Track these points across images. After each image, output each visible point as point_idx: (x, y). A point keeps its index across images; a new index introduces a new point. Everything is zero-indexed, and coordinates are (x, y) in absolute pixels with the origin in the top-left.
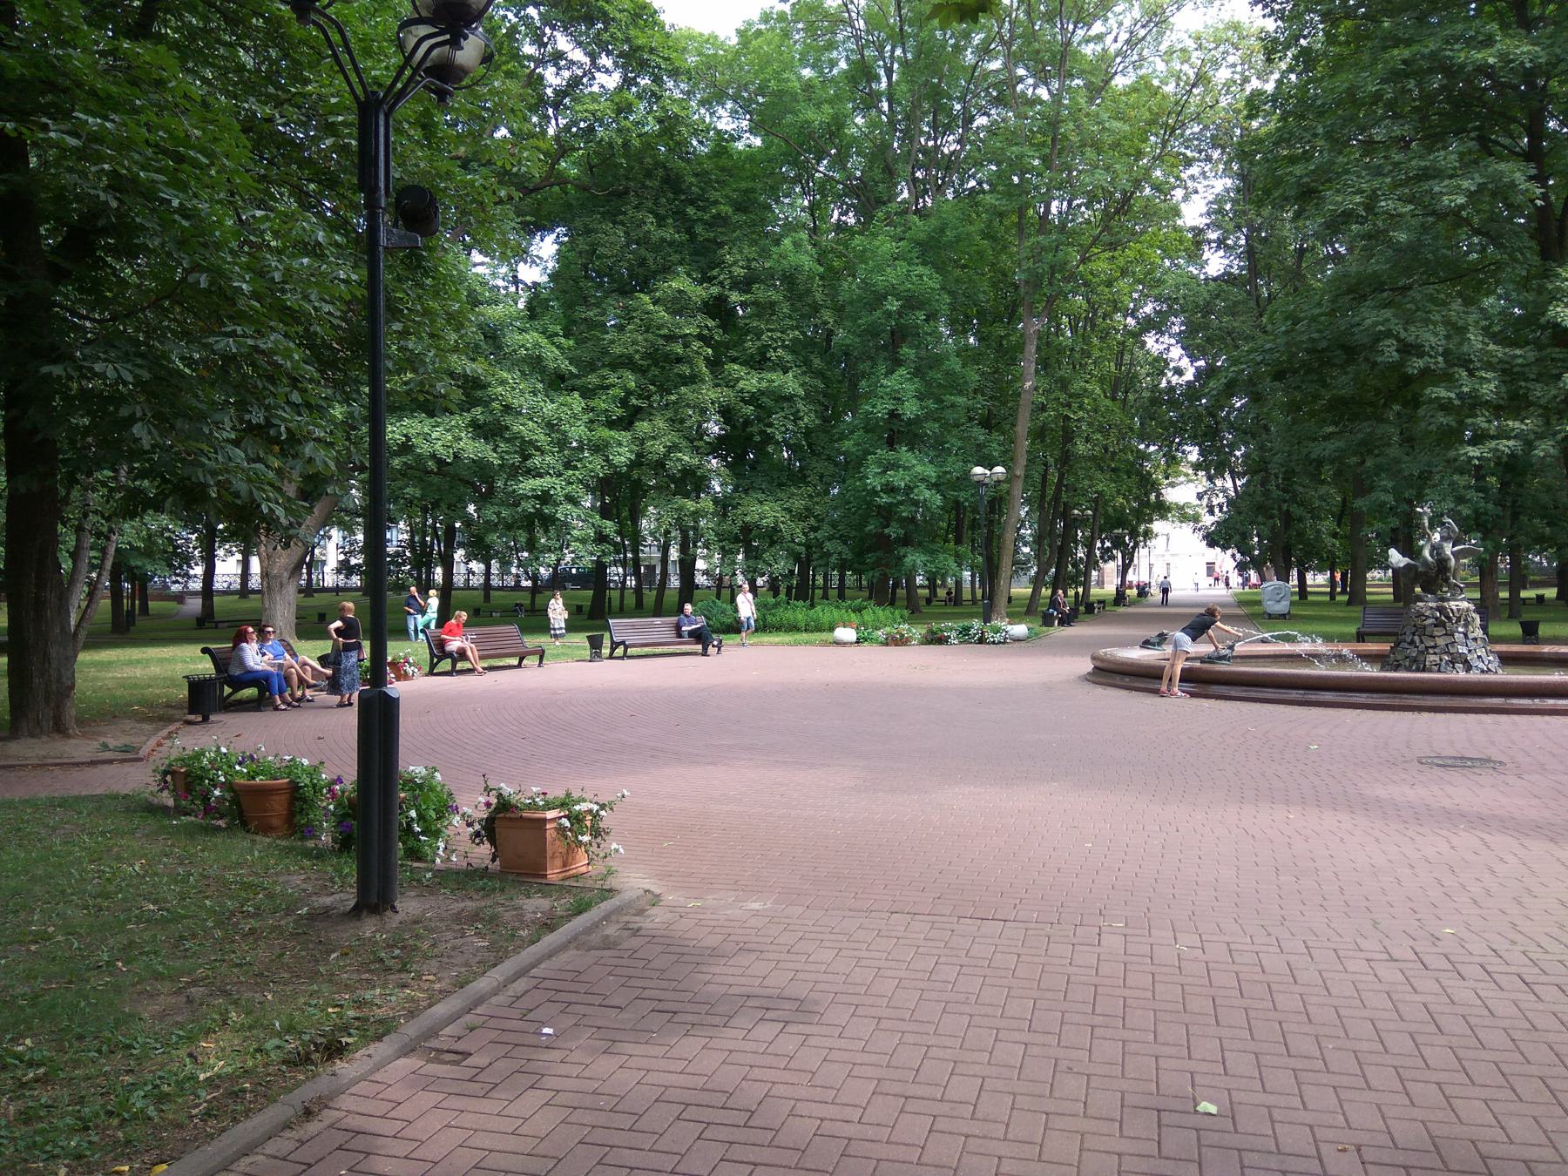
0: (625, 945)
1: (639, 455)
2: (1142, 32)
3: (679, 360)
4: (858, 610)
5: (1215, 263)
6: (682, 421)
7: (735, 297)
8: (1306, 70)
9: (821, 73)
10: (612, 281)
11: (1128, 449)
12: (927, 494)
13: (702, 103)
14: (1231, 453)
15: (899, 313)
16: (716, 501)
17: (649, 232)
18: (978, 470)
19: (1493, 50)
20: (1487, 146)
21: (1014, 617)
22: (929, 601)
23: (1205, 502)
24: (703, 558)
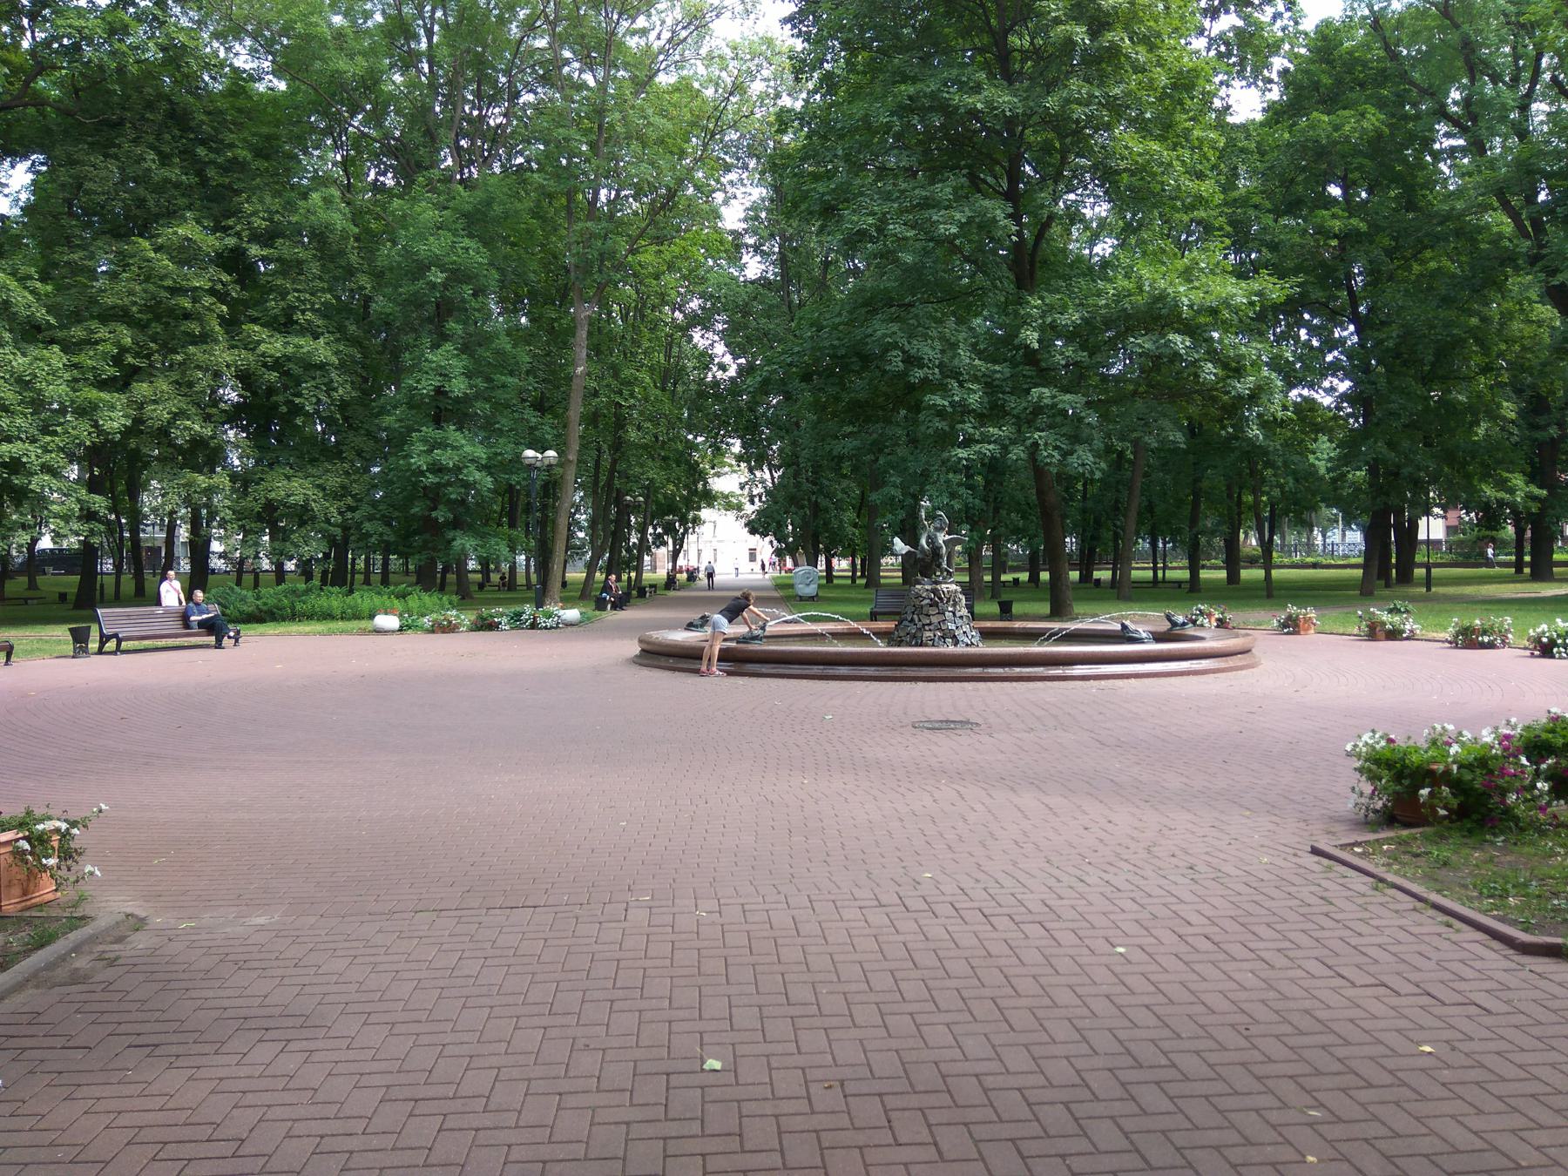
0: (99, 978)
1: (138, 421)
2: (684, 34)
3: (187, 316)
4: (403, 596)
5: (753, 267)
6: (190, 385)
7: (254, 250)
8: (828, 92)
9: (354, 23)
10: (103, 220)
11: (677, 438)
12: (478, 475)
13: (216, 35)
14: (769, 447)
15: (445, 285)
16: (234, 477)
17: (149, 170)
18: (530, 453)
19: (981, 97)
20: (976, 184)
21: (567, 602)
22: (481, 586)
23: (746, 491)
24: (220, 539)
